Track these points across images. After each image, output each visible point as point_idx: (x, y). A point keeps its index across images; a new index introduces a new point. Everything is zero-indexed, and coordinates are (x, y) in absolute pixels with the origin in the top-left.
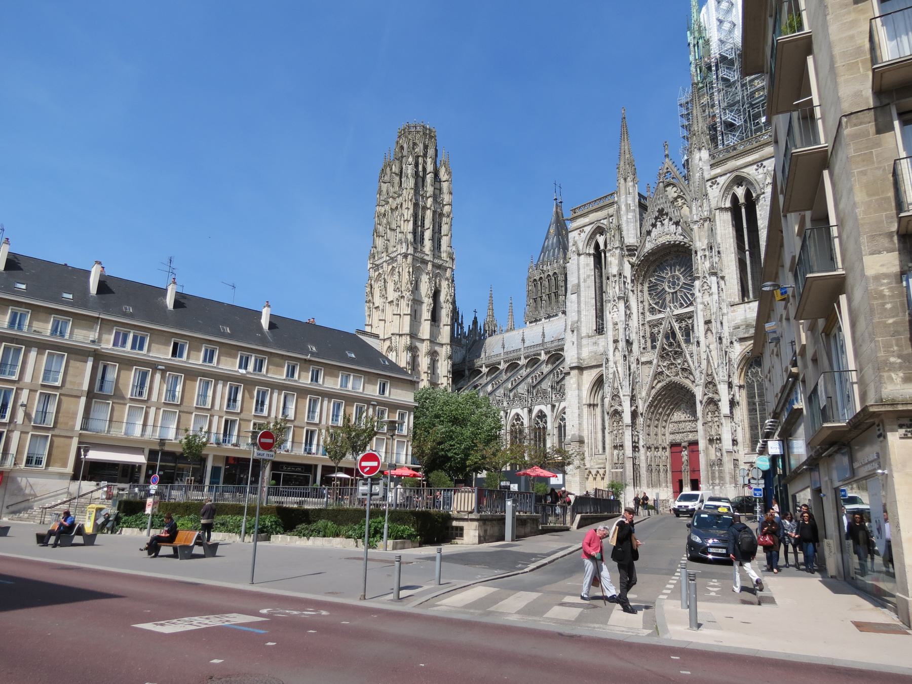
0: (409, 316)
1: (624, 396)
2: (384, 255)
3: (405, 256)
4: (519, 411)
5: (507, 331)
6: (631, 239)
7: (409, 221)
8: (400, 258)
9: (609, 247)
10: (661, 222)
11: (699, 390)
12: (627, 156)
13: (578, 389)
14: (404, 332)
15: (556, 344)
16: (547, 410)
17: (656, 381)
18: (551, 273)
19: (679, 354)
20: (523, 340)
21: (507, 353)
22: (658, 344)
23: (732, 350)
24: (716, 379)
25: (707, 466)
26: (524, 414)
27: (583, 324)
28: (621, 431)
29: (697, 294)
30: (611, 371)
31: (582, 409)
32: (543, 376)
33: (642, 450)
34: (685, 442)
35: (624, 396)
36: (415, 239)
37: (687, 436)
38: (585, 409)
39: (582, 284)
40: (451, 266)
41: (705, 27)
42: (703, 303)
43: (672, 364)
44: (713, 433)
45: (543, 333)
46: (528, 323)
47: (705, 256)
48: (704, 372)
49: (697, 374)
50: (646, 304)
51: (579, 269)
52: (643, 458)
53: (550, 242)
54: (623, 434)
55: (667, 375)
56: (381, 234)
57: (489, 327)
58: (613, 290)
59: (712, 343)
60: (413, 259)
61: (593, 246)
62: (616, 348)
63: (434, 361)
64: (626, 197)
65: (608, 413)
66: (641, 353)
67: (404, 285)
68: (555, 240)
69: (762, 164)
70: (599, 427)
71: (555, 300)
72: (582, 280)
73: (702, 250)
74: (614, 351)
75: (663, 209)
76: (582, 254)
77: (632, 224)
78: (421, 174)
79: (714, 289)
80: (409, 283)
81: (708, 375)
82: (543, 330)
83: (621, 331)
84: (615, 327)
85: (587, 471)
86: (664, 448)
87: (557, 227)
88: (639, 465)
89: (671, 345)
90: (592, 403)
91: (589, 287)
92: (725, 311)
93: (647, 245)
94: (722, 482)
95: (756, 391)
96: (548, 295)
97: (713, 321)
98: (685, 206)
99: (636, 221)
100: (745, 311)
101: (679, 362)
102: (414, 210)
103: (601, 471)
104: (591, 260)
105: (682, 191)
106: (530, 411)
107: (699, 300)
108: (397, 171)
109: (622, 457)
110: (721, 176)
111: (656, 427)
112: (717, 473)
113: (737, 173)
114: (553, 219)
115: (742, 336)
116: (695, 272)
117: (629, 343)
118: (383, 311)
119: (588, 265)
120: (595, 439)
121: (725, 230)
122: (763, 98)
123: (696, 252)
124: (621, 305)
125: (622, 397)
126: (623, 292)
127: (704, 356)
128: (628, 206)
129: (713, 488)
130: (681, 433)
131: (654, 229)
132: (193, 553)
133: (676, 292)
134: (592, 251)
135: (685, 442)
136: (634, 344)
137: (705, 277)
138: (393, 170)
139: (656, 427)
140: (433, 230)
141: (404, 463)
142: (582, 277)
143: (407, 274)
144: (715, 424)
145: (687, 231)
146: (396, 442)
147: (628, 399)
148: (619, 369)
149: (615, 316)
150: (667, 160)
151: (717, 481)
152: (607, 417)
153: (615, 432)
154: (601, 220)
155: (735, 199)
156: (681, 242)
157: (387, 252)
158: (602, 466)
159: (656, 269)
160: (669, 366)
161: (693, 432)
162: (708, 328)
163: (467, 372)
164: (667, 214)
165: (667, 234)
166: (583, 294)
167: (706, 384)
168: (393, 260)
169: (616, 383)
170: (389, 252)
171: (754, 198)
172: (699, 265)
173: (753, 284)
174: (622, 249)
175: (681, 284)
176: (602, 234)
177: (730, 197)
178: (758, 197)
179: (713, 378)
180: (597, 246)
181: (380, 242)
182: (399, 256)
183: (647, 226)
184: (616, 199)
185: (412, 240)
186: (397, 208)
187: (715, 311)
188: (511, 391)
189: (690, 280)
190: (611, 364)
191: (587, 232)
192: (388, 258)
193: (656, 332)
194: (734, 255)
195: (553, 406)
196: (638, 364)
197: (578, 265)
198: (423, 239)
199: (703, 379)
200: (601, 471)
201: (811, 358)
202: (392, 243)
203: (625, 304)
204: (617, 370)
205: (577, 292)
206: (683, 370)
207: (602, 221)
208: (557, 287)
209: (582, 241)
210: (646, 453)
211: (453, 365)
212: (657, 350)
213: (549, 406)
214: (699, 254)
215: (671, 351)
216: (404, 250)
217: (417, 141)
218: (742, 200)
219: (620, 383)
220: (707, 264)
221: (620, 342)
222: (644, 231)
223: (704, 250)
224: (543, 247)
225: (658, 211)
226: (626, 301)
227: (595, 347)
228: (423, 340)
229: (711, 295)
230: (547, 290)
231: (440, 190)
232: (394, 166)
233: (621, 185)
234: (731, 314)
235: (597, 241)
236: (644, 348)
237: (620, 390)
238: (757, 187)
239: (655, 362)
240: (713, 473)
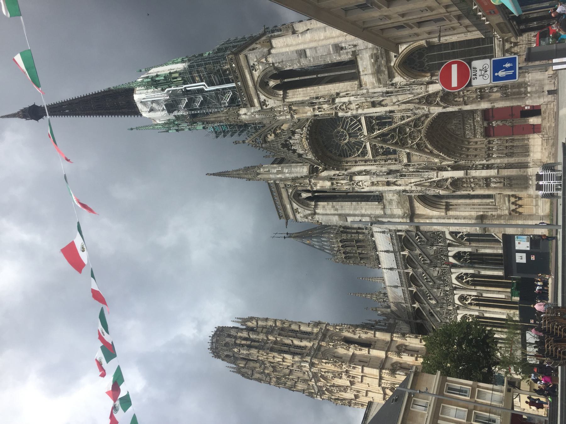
0: (365, 368)
1: (437, 177)
2: (310, 383)
3: (312, 365)
4: (454, 276)
5: (384, 283)
6: (304, 170)
7: (284, 358)
8: (314, 370)
9: (309, 188)
10: (292, 146)
11: (433, 110)
12: (241, 172)
13: (431, 218)
14: (378, 374)
15: (395, 241)
16: (453, 251)
17: (426, 150)
18: (340, 245)
19: (401, 129)
20: (391, 269)
21: (402, 284)
22: (392, 148)
23: (399, 84)
24: (424, 95)
25: (507, 99)
26: (456, 272)
27: (373, 212)
28: (472, 180)
29: (349, 114)
30: (414, 188)
31: (450, 216)
32: (423, 254)
33: (492, 161)
34: (483, 124)
35: (437, 177)
36: (300, 354)
38: (451, 213)
39: (340, 212)
40: (325, 325)
41: (168, 120)
42: (357, 109)
44: (475, 96)
45: (385, 251)
46: (380, 266)
47: (319, 108)
48: (417, 106)
49: (420, 112)
50: (358, 159)
51: (327, 214)
52: (498, 161)
53: (316, 243)
54: (474, 178)
55: (420, 140)
56: (294, 384)
57: (381, 298)
58: (344, 185)
59: (392, 100)
60: (316, 357)
63: (406, 350)
64: (271, 173)
65: (454, 192)
66: (400, 162)
67: (336, 369)
68: (315, 240)
69: (252, 67)
70: (468, 201)
71: (362, 243)
72: (336, 212)
73: (314, 111)
74: (397, 185)
75: (282, 144)
77: (293, 169)
78: (249, 343)
79: (346, 100)
80: (335, 364)
81: (419, 103)
82: (382, 251)
83: (379, 179)
84: (376, 184)
86: (489, 142)
87: (305, 238)
88: (506, 164)
89: (393, 137)
90: (444, 207)
91: (342, 207)
92: (365, 91)
93: (309, 157)
94: (523, 85)
95: (437, 62)
96: (357, 248)
97: (372, 100)
98: (282, 127)
99: (291, 166)
100: (366, 75)
101: (408, 129)
102: (276, 352)
103: (513, 200)
104: (321, 204)
105: (270, 130)
106: (454, 266)
107: (354, 112)
108: (244, 362)
109: (498, 179)
112: (514, 90)
113: (258, 85)
114: (299, 240)
116: (331, 116)
117: (390, 172)
118: (358, 392)
119: (324, 207)
120: (480, 205)
121: (300, 94)
122: (216, 76)
123: (315, 116)
124: (357, 178)
125: (439, 179)
126: (346, 177)
127: (404, 107)
128: (278, 172)
129: (529, 93)
130: (474, 128)
131: (297, 152)
133: (349, 134)
134: (313, 203)
135: (483, 124)
136: (391, 169)
137: (336, 108)
138: (242, 365)
139: (468, 149)
140: (294, 337)
141: (502, 394)
142: (333, 212)
143: (327, 365)
144: (465, 94)
145: (300, 124)
146: (478, 400)
147: (440, 173)
148: (413, 181)
149: (365, 184)
150: (247, 142)
151: (523, 90)
152: (458, 193)
153: (473, 185)
154: (288, 195)
156: (308, 129)
157: (307, 380)
158: (507, 199)
159: (329, 150)
162: (378, 104)
163: (419, 321)
165: (301, 141)
166: (347, 212)
167: (428, 103)
168: (315, 375)
169: (426, 184)
170: (308, 378)
171: (277, 72)
172: (325, 113)
173: (491, 303)
174: (311, 177)
175: (342, 130)
176: (300, 195)
178: (276, 68)
179: (423, 97)
180: (308, 198)
181: (300, 386)
182: (312, 370)
183: (295, 157)
184: (272, 181)
185: (300, 356)
186: (273, 367)
187: (363, 98)
188: (435, 283)
189: (339, 123)
190: (408, 188)
191: (297, 207)
192: (313, 380)
193: (382, 150)
194: (320, 87)
195: (450, 245)
196: (409, 165)
197: (323, 215)
198: (300, 347)
199: (423, 106)
200: (513, 200)
202: (301, 375)
203: (356, 175)
204: (413, 183)
205: (344, 217)
206: (415, 126)
207: (289, 194)
208: (352, 240)
209: (304, 211)
210: (494, 158)
211: (412, 332)
212: (398, 149)
213: (449, 249)
214: (317, 113)
215: (399, 137)
216: (307, 365)
217: (224, 342)
218: (278, 82)
219: (426, 180)
220: (325, 106)
221: (389, 179)
222: (298, 160)
224: (320, 249)
225: (283, 148)
226: (354, 174)
227: (394, 203)
228: (387, 357)
229: (350, 103)
230: (354, 248)
231: (263, 327)
232: (240, 365)
233: (262, 178)
234: (368, 87)
236: (396, 161)
237: (432, 180)
238: (269, 69)
239: (408, 151)
240: (514, 94)
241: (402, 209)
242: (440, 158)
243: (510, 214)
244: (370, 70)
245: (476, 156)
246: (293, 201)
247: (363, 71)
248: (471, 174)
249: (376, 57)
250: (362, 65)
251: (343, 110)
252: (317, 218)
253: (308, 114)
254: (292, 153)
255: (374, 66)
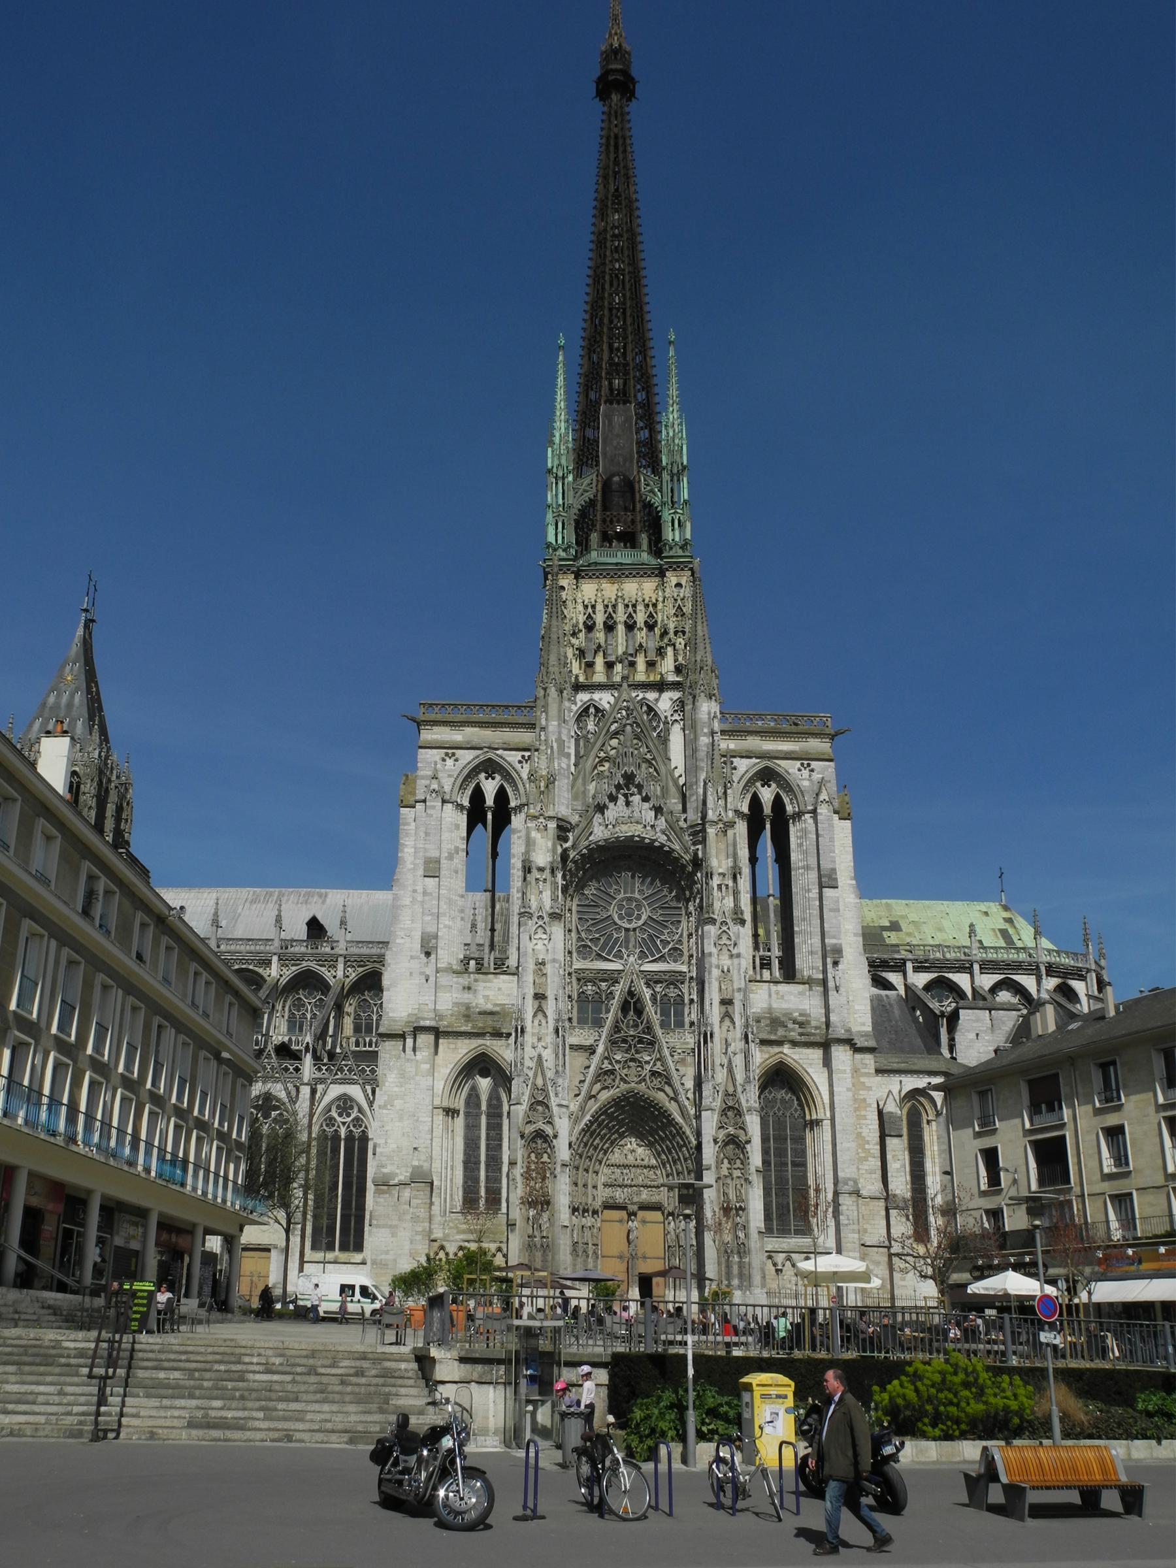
30: (529, 1052)
35: (560, 1105)
37: (639, 1194)
43: (633, 1060)
48: (722, 1089)
61: (469, 792)
62: (540, 1010)
76: (449, 802)
81: (727, 1094)
85: (436, 1245)
100: (770, 995)
110: (742, 757)
111: (587, 1171)
113: (769, 764)
115: (764, 1036)
125: (555, 1109)
130: (626, 1186)
132: (1004, 1502)
134: (466, 803)
139: (587, 1171)
149: (540, 946)
154: (497, 749)
155: (755, 802)
160: (626, 1062)
161: (650, 1187)
164: (640, 787)
177: (749, 796)
199: (719, 1100)
201: (489, 1052)
207: (499, 752)
209: (450, 776)
223: (724, 875)
227: (466, 996)
235: (478, 784)
239: (600, 1049)
241: (450, 1012)
242: (578, 1114)
243: (434, 1241)
244: (780, 1006)
245: (576, 1184)
246: (478, 757)
247: (777, 993)
248: (563, 1175)
249: (803, 1024)
250: (790, 993)
251: (720, 938)
252: (433, 804)
253: (715, 860)
254: (611, 793)
255: (785, 1015)
